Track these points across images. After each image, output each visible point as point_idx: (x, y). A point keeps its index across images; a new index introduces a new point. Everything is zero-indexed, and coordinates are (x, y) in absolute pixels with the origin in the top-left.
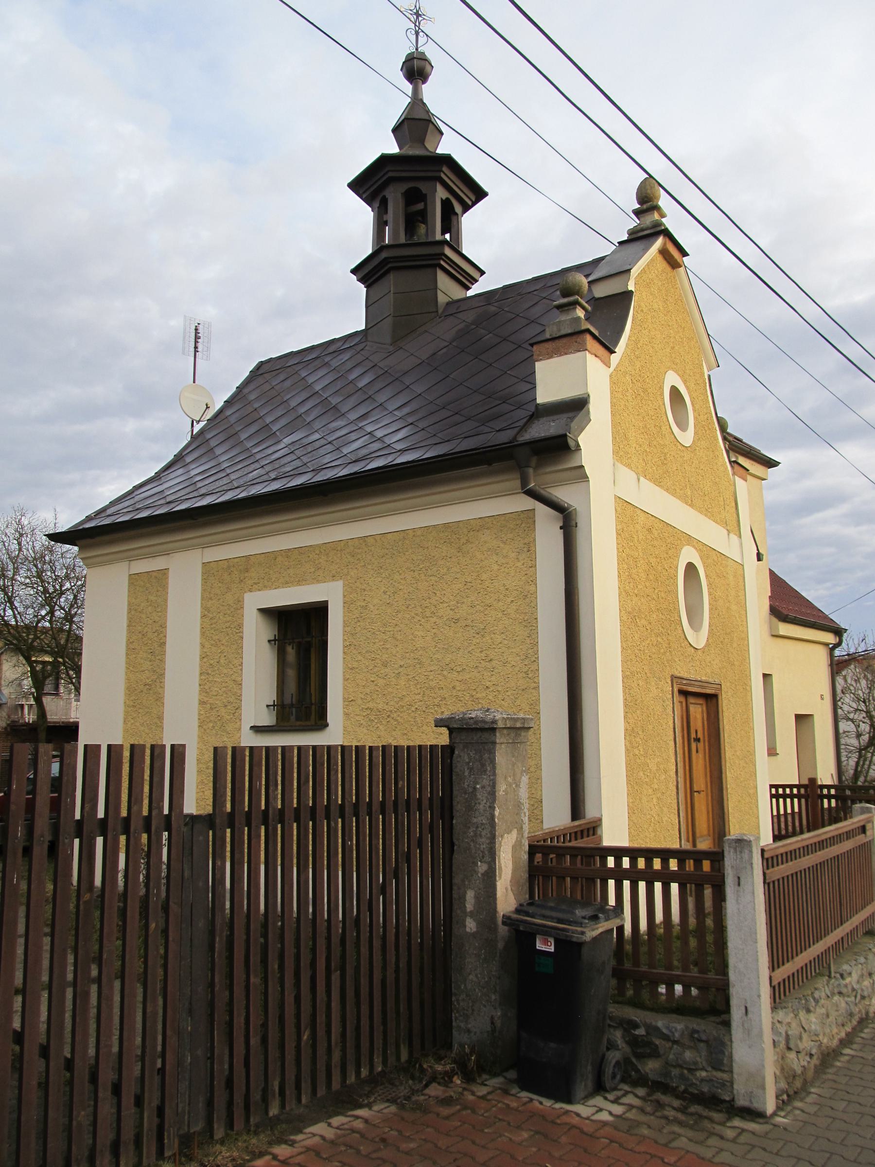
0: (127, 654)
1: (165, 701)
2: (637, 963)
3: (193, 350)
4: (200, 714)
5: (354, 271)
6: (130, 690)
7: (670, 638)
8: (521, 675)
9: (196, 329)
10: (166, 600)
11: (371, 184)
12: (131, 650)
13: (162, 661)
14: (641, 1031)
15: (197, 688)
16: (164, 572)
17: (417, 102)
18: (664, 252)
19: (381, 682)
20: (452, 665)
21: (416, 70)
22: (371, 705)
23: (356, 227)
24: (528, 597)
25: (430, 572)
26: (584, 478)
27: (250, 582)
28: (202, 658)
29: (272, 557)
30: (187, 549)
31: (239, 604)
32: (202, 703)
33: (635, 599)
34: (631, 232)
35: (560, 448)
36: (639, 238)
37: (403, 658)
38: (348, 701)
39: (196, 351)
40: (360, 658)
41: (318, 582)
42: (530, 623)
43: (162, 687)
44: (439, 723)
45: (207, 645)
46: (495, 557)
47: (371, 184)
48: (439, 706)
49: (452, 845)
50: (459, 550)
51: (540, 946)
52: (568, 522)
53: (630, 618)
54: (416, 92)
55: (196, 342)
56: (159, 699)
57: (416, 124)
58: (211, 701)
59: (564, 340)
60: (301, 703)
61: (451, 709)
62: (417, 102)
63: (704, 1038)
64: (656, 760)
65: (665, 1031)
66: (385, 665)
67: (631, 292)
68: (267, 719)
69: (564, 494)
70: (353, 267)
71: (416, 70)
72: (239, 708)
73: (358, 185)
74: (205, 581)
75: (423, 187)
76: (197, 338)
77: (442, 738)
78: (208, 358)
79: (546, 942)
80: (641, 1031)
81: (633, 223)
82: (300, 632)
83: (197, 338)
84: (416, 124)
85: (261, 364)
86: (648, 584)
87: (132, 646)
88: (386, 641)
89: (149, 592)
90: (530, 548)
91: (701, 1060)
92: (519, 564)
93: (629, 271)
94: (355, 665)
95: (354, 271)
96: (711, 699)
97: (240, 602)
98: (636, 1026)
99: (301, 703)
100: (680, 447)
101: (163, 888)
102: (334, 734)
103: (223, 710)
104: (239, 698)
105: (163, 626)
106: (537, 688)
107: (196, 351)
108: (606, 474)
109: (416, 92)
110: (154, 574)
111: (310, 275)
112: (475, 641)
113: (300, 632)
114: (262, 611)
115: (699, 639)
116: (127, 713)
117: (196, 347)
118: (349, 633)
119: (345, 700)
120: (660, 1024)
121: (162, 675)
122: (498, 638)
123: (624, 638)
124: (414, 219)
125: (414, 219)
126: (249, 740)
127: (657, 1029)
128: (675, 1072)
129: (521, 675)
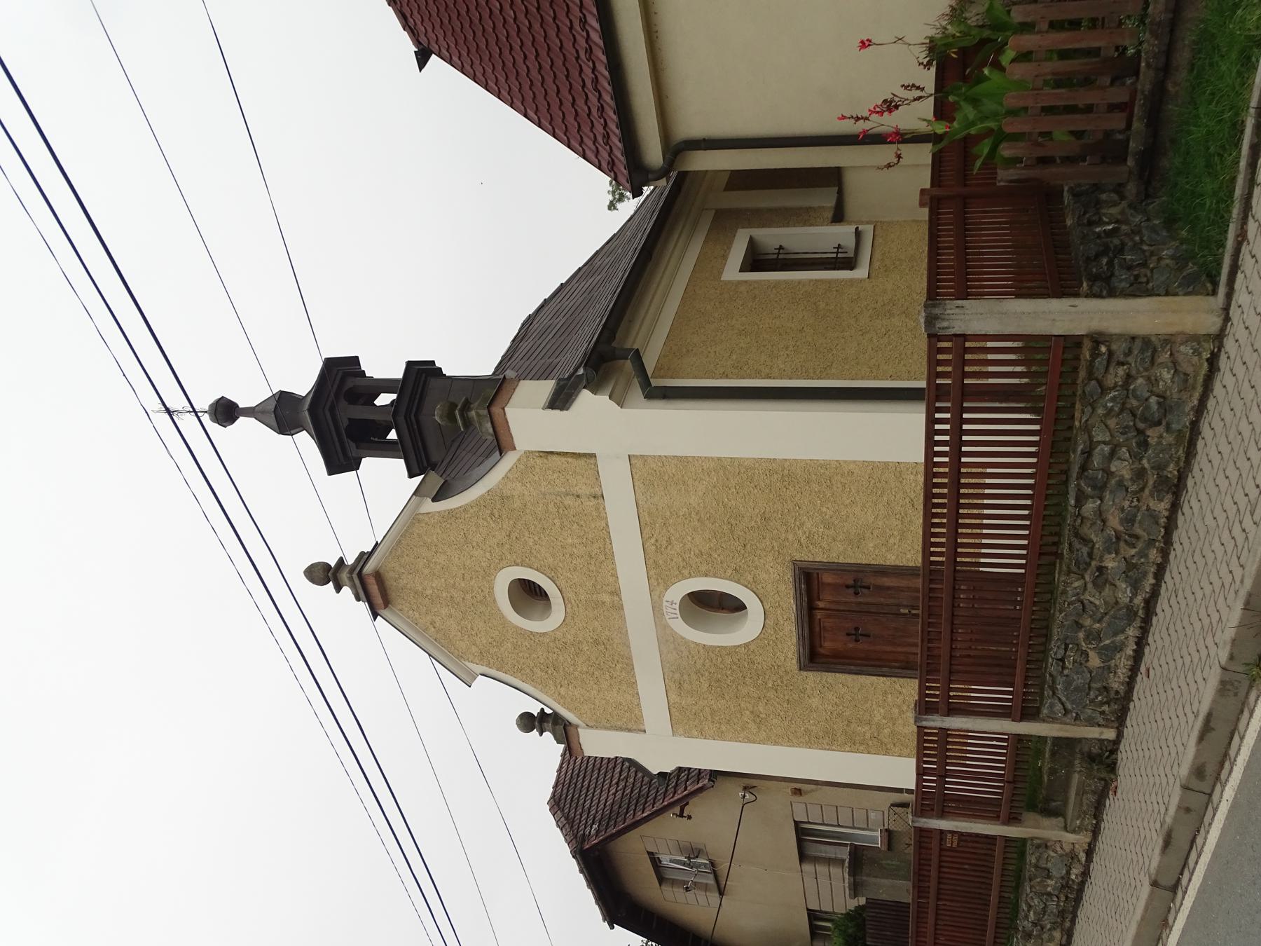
18: (387, 603)
21: (225, 412)
54: (249, 412)
57: (283, 413)
71: (225, 412)
84: (283, 413)
109: (249, 412)
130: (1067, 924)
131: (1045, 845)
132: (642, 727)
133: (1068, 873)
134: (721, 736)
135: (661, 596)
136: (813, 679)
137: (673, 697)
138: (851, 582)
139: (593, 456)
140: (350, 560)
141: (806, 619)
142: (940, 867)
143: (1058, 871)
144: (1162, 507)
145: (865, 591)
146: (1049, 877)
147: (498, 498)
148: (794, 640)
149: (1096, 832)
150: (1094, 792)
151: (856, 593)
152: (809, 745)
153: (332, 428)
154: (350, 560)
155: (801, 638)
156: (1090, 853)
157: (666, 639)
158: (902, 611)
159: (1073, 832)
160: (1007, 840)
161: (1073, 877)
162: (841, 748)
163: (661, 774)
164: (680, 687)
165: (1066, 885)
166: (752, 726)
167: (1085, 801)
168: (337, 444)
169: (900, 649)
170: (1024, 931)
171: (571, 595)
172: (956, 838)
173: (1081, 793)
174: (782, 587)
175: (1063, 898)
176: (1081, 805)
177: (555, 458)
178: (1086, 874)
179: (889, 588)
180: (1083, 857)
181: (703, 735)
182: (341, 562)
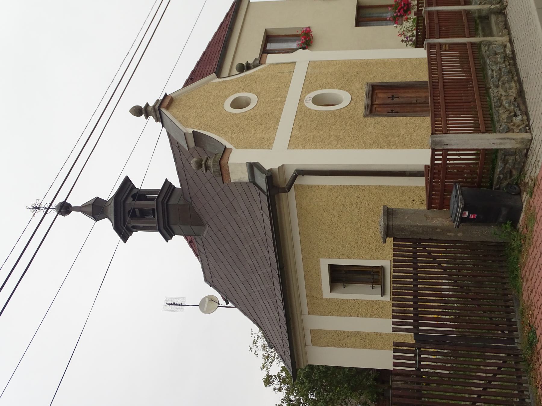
0: (348, 347)
1: (369, 331)
2: (476, 178)
3: (181, 306)
4: (376, 317)
5: (167, 241)
6: (364, 347)
7: (347, 117)
8: (364, 192)
9: (169, 304)
10: (324, 330)
11: (124, 231)
12: (346, 346)
13: (351, 332)
14: (502, 176)
15: (364, 319)
16: (312, 331)
17: (81, 209)
18: (167, 108)
19: (364, 245)
20: (358, 217)
21: (65, 209)
22: (374, 248)
23: (147, 240)
24: (331, 188)
25: (318, 224)
26: (283, 166)
27: (318, 295)
28: (351, 316)
29: (307, 286)
30: (302, 320)
31: (328, 300)
32: (370, 317)
33: (331, 139)
34: (157, 120)
35: (270, 176)
36: (160, 118)
37: (354, 236)
38: (372, 258)
39: (181, 305)
40: (353, 253)
41: (320, 268)
42: (342, 188)
43: (363, 332)
44: (385, 242)
45: (345, 313)
46: (314, 200)
47: (124, 231)
48: (375, 223)
49: (430, 239)
50: (309, 213)
51: (466, 216)
52: (301, 173)
53: (340, 143)
55: (177, 305)
56: (368, 334)
57: (96, 209)
58: (370, 312)
59: (223, 171)
60: (371, 276)
61: (380, 236)
62: (81, 209)
63: (503, 157)
64: (401, 129)
65: (501, 168)
66: (357, 243)
67: (193, 131)
68: (379, 289)
69: (290, 173)
70: (165, 241)
72: (373, 301)
73: (125, 238)
74: (317, 314)
75: (128, 208)
76: (174, 304)
77: (390, 240)
78: (185, 299)
79: (465, 214)
80: (502, 176)
81: (151, 118)
82: (340, 276)
83: (174, 304)
84: (96, 209)
85: (206, 280)
86: (324, 130)
87: (344, 345)
88: (347, 242)
89: (324, 338)
90: (310, 187)
91: (513, 158)
92: (317, 191)
93: (184, 133)
94: (356, 254)
95: (167, 241)
96: (374, 89)
97: (327, 300)
98: (499, 177)
99: (371, 276)
100: (259, 103)
101: (492, 289)
102: (387, 263)
103: (374, 308)
104: (369, 301)
105: (336, 331)
106: (369, 186)
107: (181, 305)
108: (279, 155)
110: (312, 335)
111: (168, 262)
112: (348, 208)
113: (340, 276)
114: (331, 291)
115: (345, 97)
116: (374, 348)
117: (179, 305)
118: (343, 256)
119: (371, 259)
120: (499, 170)
121: (358, 332)
122: (348, 200)
123: (349, 147)
124: (143, 213)
125: (143, 213)
126: (388, 298)
127: (500, 171)
128: (516, 166)
129: (364, 192)
130: (516, 78)
131: (490, 44)
132: (271, 148)
133: (505, 51)
134: (316, 148)
135: (304, 97)
136: (370, 120)
137: (295, 132)
138: (391, 96)
139: (295, 62)
140: (151, 104)
141: (370, 98)
142: (444, 85)
143: (500, 50)
144: (505, 39)
146: (496, 54)
147: (250, 75)
148: (363, 107)
149: (509, 34)
150: (502, 22)
151: (393, 99)
152: (365, 148)
153: (127, 192)
154: (151, 104)
156: (511, 42)
157: (302, 111)
159: (500, 36)
160: (472, 44)
161: (508, 52)
162: (382, 148)
163: (271, 170)
164: (300, 127)
165: (505, 57)
166: (335, 142)
167: (500, 26)
168: (122, 209)
170: (494, 84)
171: (262, 100)
172: (447, 46)
173: (497, 24)
174: (361, 91)
175: (508, 64)
176: (499, 27)
177: (280, 65)
178: (513, 51)
179: (407, 97)
180: (508, 45)
181: (304, 147)
182: (147, 105)
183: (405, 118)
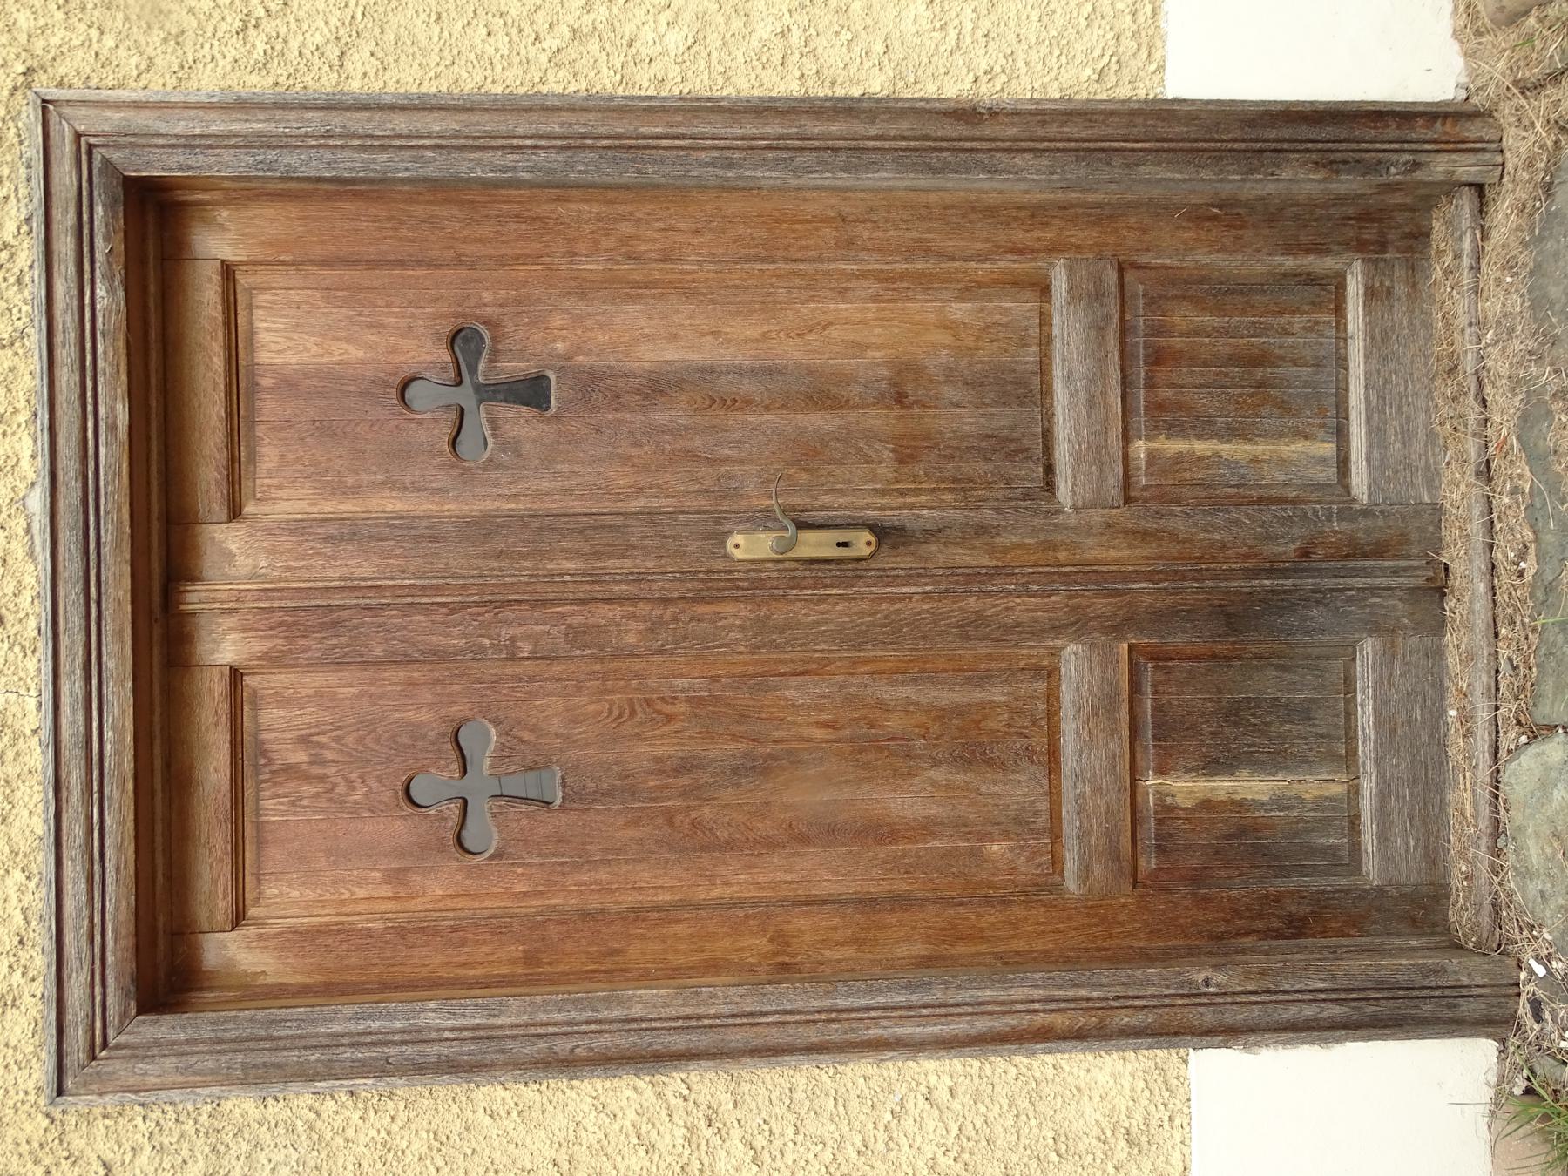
132: (1344, 795)
145: (517, 419)
155: (1345, 301)
158: (745, 546)
169: (737, 880)
183: (629, 1094)
